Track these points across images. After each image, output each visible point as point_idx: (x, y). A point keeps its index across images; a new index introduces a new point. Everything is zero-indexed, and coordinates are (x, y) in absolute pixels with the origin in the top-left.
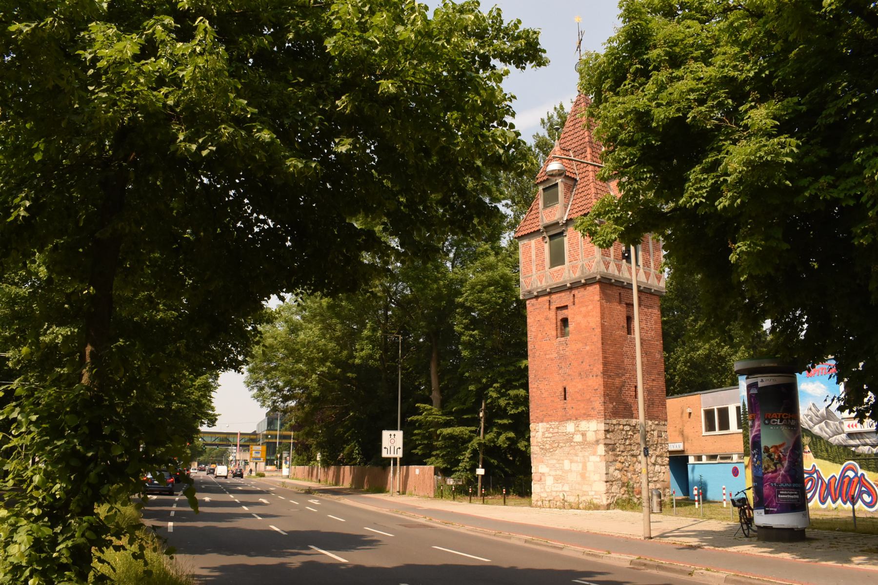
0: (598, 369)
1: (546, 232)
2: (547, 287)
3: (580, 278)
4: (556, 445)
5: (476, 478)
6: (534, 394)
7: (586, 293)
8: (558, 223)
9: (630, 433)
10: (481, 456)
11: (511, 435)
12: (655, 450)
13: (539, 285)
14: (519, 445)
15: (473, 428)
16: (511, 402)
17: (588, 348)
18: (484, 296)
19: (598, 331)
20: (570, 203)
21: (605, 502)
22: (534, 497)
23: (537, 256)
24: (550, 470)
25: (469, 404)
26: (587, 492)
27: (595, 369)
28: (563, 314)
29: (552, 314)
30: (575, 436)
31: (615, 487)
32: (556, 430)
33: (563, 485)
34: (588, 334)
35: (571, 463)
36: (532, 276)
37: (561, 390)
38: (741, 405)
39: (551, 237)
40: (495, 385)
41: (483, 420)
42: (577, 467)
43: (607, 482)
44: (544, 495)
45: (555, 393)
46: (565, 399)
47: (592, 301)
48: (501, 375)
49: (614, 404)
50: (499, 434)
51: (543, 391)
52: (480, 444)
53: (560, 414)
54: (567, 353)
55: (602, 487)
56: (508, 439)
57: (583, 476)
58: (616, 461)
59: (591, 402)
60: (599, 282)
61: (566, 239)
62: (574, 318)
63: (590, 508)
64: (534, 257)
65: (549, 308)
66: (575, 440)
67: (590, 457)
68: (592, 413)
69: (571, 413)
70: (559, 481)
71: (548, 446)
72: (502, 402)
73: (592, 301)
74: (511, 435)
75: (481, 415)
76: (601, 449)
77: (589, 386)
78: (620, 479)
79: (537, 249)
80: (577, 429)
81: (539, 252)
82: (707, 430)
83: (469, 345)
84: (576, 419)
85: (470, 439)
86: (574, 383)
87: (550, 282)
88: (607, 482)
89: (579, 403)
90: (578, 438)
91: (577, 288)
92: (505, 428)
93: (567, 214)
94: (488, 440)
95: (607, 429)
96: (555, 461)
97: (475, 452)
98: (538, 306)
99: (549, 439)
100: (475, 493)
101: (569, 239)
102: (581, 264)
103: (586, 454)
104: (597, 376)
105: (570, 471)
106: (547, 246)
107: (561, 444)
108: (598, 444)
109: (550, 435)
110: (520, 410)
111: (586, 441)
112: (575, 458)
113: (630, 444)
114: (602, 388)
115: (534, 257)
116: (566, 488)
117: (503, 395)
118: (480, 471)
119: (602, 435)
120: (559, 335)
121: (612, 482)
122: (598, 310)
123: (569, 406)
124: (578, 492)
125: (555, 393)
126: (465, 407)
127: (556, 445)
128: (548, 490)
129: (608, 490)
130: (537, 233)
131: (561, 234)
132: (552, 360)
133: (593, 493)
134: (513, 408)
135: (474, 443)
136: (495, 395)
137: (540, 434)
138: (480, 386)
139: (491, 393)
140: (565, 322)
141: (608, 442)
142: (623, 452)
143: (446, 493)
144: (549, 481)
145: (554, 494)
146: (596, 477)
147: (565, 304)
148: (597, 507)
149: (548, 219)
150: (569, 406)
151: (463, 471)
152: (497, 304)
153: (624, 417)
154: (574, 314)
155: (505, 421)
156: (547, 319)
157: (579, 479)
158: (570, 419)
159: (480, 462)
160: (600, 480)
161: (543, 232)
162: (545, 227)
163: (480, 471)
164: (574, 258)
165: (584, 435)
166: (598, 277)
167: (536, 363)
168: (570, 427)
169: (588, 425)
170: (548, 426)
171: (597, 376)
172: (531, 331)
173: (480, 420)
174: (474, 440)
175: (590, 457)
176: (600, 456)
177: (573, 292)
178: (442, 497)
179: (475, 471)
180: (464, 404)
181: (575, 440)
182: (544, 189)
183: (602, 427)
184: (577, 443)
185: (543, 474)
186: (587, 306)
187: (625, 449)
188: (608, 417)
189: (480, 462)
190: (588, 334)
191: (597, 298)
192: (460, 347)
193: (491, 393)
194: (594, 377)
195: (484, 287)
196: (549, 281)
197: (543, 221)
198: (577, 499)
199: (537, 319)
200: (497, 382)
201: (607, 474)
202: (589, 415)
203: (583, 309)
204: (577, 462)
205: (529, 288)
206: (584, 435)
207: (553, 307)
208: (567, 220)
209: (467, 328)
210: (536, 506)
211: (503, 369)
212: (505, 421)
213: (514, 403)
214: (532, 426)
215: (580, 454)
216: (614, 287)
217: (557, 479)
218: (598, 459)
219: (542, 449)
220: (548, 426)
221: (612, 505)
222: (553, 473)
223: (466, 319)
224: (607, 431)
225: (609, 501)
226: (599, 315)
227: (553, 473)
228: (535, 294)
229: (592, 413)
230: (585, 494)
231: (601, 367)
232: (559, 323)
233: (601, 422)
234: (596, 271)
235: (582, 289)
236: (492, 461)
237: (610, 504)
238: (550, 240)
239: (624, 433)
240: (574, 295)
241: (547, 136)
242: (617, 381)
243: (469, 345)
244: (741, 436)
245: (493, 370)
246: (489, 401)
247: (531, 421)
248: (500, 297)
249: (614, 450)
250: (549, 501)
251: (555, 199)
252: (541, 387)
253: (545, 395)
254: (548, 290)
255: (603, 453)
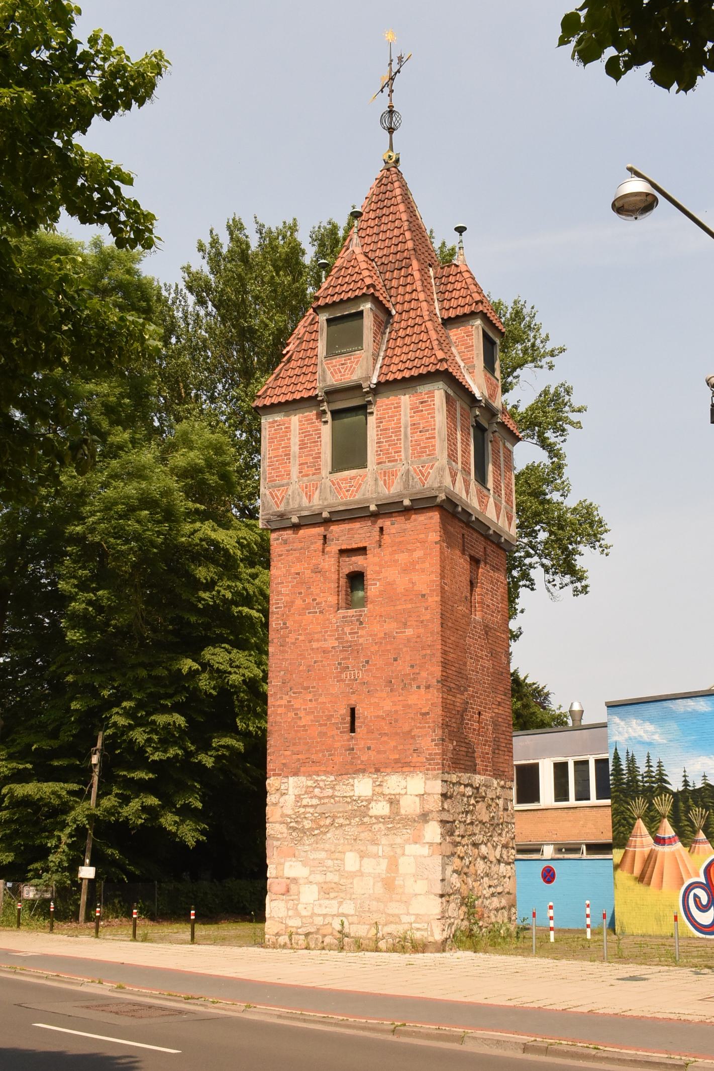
0: (431, 674)
1: (328, 402)
2: (323, 509)
3: (400, 495)
4: (328, 821)
5: (77, 884)
6: (278, 719)
7: (408, 525)
8: (359, 387)
9: (472, 801)
10: (89, 844)
11: (152, 801)
12: (500, 834)
13: (305, 502)
14: (162, 820)
15: (75, 787)
16: (155, 737)
17: (409, 632)
18: (132, 525)
19: (434, 599)
20: (382, 354)
21: (438, 937)
22: (270, 927)
23: (302, 446)
24: (312, 872)
25: (66, 737)
26: (398, 916)
27: (424, 674)
28: (357, 563)
29: (329, 563)
30: (373, 804)
31: (453, 905)
32: (329, 792)
33: (341, 903)
34: (410, 606)
35: (362, 857)
36: (288, 484)
37: (344, 711)
38: (610, 756)
39: (336, 414)
40: (125, 704)
41: (97, 770)
42: (376, 867)
43: (442, 896)
44: (294, 923)
45: (330, 717)
46: (353, 730)
47: (423, 542)
48: (139, 684)
49: (455, 743)
50: (125, 800)
51: (302, 714)
52: (91, 818)
53: (339, 759)
54: (361, 641)
55: (434, 906)
56: (145, 809)
57: (389, 884)
58: (453, 854)
59: (413, 737)
60: (440, 507)
61: (371, 420)
62: (379, 572)
63: (403, 950)
64: (295, 448)
65: (323, 552)
66: (372, 812)
67: (407, 847)
68: (415, 759)
69: (364, 758)
70: (332, 895)
71: (307, 824)
72: (139, 736)
73: (423, 542)
74: (152, 801)
75: (95, 759)
76: (433, 831)
77: (410, 706)
78: (458, 891)
79: (305, 433)
80: (377, 789)
81: (308, 442)
82: (520, 800)
83: (81, 621)
84: (377, 770)
85: (66, 808)
86: (373, 700)
87: (331, 500)
88: (442, 896)
89: (385, 738)
90: (381, 808)
91: (389, 515)
92: (142, 787)
93: (377, 373)
94: (106, 810)
95: (445, 791)
96: (323, 855)
97: (80, 832)
98: (297, 545)
99: (311, 810)
100: (75, 917)
101: (380, 421)
102: (403, 469)
103: (398, 840)
104: (428, 687)
105: (360, 873)
106: (326, 431)
107: (341, 821)
108: (427, 821)
109: (315, 801)
110: (172, 752)
111: (398, 814)
112: (373, 849)
113: (472, 823)
114: (439, 710)
115: (295, 448)
116: (348, 908)
117: (140, 723)
118: (87, 872)
119: (434, 803)
120: (342, 604)
121: (449, 895)
122: (436, 560)
123: (362, 744)
124: (375, 917)
125: (330, 717)
126: (55, 744)
127: (328, 821)
128: (304, 913)
129: (443, 912)
130: (311, 401)
131: (363, 409)
132: (325, 651)
133: (413, 918)
134: (156, 749)
135: (79, 814)
136: (122, 721)
137: (290, 799)
138: (94, 702)
139: (115, 718)
140: (356, 579)
141: (446, 817)
142: (463, 837)
143: (26, 915)
144: (308, 895)
145: (319, 921)
146: (420, 887)
147: (361, 545)
148: (420, 947)
149: (338, 376)
150: (362, 744)
151: (57, 871)
152: (153, 544)
153: (466, 770)
154: (381, 566)
155: (141, 775)
156: (317, 571)
157: (379, 889)
158: (364, 771)
159: (88, 854)
160: (428, 892)
161: (322, 401)
162: (327, 393)
163: (87, 872)
164: (388, 456)
165: (393, 802)
166: (442, 496)
167: (286, 656)
168: (363, 786)
169: (403, 783)
170: (310, 783)
171: (428, 687)
172: (279, 593)
173: (92, 771)
174: (78, 809)
175: (407, 847)
176: (431, 844)
177: (380, 522)
178: (19, 924)
179: (77, 872)
180: (54, 735)
181: (372, 812)
182: (329, 321)
183: (437, 787)
184: (376, 817)
185: (295, 880)
186: (410, 551)
187: (466, 831)
188: (447, 769)
189: (88, 854)
190: (410, 606)
191: (434, 536)
192: (63, 623)
193: (115, 718)
194: (423, 690)
195: (132, 510)
196: (329, 496)
197: (324, 380)
198: (374, 931)
199: (293, 570)
200: (129, 698)
201: (443, 880)
202: (407, 764)
203: (402, 557)
204: (376, 856)
205: (281, 508)
206: (393, 802)
207: (333, 548)
208: (379, 384)
209: (83, 586)
210: (274, 946)
211: (143, 673)
212: (141, 775)
213: (160, 740)
214: (272, 783)
215: (384, 841)
216: (456, 521)
217: (326, 891)
218: (425, 851)
219: (294, 829)
220: (310, 783)
221: (449, 942)
222: (319, 878)
223: (84, 568)
224: (444, 796)
225: (445, 935)
226: (437, 569)
227: (319, 878)
228: (295, 520)
229: (415, 759)
230: (395, 919)
231: (437, 671)
232: (343, 581)
233: (435, 777)
234: (436, 485)
235: (401, 519)
236: (109, 851)
237: (447, 939)
238: (333, 419)
239: (465, 799)
240: (381, 529)
241: (206, 269)
242: (459, 699)
243: (81, 621)
244: (609, 811)
245: (124, 675)
246: (109, 732)
247: (269, 773)
248: (159, 533)
249: (451, 833)
250: (307, 935)
251: (356, 340)
252: (296, 704)
253: (306, 720)
254: (325, 515)
255: (438, 839)
